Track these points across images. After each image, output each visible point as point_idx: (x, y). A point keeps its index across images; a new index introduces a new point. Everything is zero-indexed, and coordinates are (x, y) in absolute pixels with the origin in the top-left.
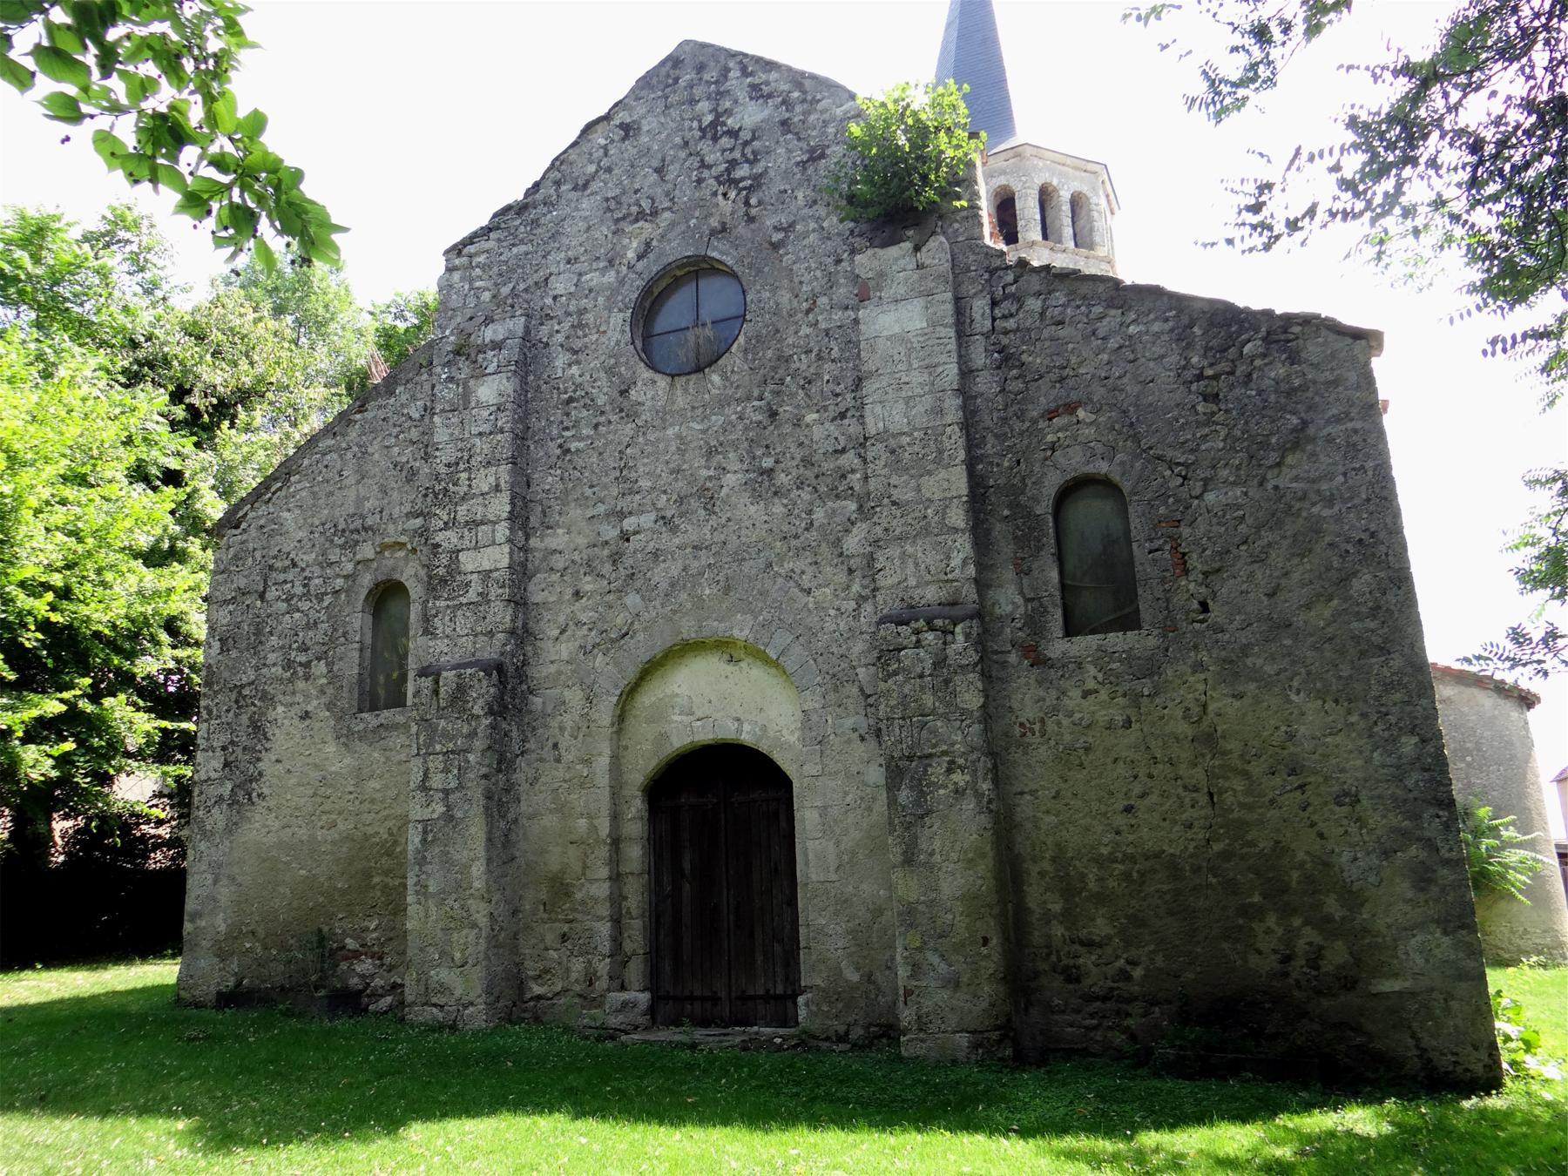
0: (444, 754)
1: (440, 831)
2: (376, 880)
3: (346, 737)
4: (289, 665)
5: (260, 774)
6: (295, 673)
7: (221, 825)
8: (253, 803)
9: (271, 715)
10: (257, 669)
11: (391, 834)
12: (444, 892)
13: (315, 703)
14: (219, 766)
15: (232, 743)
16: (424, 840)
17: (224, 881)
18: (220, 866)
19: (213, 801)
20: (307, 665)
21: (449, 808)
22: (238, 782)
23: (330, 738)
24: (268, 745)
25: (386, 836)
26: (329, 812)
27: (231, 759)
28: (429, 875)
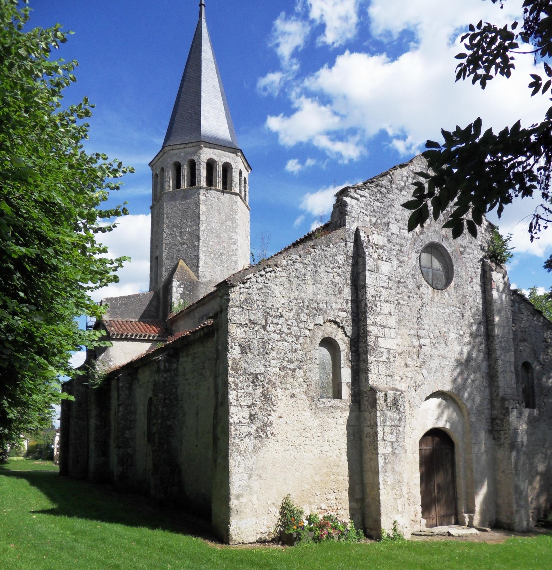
4: (282, 368)
5: (271, 423)
6: (287, 373)
7: (250, 448)
8: (269, 438)
14: (247, 415)
15: (253, 404)
16: (385, 462)
17: (254, 478)
19: (244, 435)
20: (294, 370)
24: (274, 408)
27: (253, 413)
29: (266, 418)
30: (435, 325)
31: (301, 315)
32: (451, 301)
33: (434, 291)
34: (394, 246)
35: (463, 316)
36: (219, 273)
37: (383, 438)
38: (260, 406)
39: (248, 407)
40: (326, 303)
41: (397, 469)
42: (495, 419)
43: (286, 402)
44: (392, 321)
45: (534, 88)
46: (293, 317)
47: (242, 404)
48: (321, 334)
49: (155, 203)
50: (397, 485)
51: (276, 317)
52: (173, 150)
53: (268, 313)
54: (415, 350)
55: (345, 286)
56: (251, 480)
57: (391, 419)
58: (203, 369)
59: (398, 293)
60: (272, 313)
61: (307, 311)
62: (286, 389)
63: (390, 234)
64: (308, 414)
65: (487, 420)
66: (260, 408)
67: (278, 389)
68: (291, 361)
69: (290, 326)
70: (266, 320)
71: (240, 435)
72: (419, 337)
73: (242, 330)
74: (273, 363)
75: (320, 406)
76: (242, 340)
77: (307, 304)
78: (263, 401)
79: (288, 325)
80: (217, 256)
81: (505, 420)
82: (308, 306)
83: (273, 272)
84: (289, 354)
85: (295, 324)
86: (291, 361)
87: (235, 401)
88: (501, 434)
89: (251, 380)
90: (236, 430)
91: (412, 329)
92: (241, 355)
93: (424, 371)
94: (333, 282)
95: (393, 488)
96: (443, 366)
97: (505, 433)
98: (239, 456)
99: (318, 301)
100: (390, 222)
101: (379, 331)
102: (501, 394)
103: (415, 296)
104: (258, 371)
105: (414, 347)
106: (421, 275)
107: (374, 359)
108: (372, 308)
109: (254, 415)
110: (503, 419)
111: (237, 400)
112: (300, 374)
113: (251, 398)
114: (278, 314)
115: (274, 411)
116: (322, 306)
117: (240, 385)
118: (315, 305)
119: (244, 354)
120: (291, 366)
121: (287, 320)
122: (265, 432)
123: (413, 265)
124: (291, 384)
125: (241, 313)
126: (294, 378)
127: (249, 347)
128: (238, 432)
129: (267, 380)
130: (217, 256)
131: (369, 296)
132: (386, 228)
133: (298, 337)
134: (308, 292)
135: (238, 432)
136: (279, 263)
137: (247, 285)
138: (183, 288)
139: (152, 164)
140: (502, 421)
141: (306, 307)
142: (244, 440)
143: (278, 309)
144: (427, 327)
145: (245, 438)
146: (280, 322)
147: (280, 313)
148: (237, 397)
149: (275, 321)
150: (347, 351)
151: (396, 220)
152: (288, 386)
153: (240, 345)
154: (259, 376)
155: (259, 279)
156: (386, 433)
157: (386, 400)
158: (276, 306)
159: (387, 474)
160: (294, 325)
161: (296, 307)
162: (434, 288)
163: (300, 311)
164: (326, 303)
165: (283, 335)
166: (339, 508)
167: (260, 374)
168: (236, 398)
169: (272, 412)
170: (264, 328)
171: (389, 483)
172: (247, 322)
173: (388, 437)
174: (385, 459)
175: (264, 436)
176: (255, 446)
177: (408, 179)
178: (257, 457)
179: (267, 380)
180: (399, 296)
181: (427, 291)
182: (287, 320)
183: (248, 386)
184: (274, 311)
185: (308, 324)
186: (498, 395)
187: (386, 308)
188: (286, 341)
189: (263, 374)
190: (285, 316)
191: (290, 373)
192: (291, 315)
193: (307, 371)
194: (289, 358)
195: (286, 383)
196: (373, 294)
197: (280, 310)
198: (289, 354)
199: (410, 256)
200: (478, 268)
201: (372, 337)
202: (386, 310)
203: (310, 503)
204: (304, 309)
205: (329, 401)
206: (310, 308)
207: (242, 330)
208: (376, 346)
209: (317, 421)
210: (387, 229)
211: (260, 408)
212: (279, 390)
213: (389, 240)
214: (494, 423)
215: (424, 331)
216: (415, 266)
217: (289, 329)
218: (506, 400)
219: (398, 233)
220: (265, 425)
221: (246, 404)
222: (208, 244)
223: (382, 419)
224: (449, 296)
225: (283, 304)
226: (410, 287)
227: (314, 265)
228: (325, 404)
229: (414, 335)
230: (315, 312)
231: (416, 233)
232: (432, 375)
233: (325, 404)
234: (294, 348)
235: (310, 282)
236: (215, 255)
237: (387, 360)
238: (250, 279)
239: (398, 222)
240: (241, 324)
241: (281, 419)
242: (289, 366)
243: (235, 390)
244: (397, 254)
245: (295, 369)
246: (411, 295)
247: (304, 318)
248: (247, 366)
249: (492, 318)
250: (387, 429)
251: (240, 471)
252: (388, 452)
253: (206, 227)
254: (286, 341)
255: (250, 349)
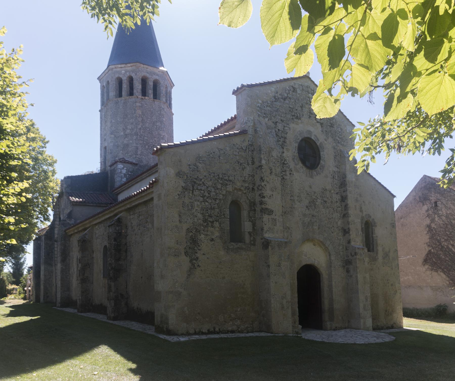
20: (212, 222)
24: (199, 248)
31: (217, 184)
34: (280, 139)
36: (152, 159)
45: (435, 5)
48: (231, 197)
49: (103, 107)
52: (116, 68)
53: (195, 182)
58: (147, 223)
59: (283, 171)
61: (221, 182)
62: (207, 235)
63: (277, 130)
68: (210, 216)
70: (193, 187)
75: (230, 247)
77: (221, 176)
80: (150, 147)
82: (222, 178)
85: (213, 190)
86: (210, 216)
100: (277, 122)
112: (217, 224)
115: (199, 250)
118: (227, 178)
121: (207, 187)
130: (150, 147)
131: (133, 323)
133: (215, 199)
138: (126, 169)
139: (100, 78)
143: (201, 179)
146: (203, 188)
149: (199, 187)
160: (213, 191)
163: (216, 181)
165: (205, 198)
177: (289, 92)
180: (284, 173)
182: (207, 187)
188: (207, 202)
194: (209, 213)
195: (207, 231)
204: (219, 180)
205: (237, 244)
206: (223, 180)
213: (277, 134)
217: (209, 194)
219: (283, 130)
222: (143, 138)
234: (212, 207)
236: (149, 146)
239: (283, 122)
242: (209, 219)
244: (282, 144)
253: (142, 126)
254: (207, 202)
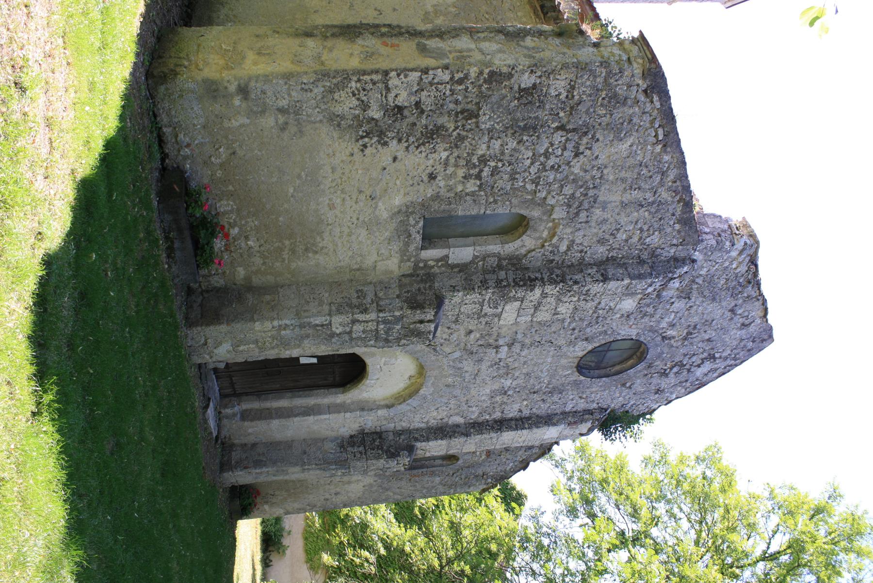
0: (377, 330)
1: (323, 332)
2: (287, 243)
3: (406, 211)
4: (483, 160)
5: (385, 144)
6: (475, 166)
7: (338, 109)
8: (357, 141)
9: (441, 147)
10: (490, 131)
11: (322, 248)
12: (281, 338)
13: (442, 184)
14: (400, 101)
15: (422, 112)
16: (317, 325)
17: (281, 119)
18: (296, 113)
19: (364, 98)
20: (478, 177)
21: (339, 335)
22: (381, 124)
23: (409, 198)
24: (412, 148)
25: (321, 245)
26: (343, 205)
27: (406, 112)
28: (293, 330)
29: (394, 135)
30: (525, 363)
32: (557, 378)
33: (577, 357)
35: (534, 393)
37: (358, 321)
38: (418, 123)
39: (418, 104)
40: (587, 222)
41: (306, 342)
42: (380, 437)
43: (423, 167)
44: (543, 316)
46: (573, 173)
47: (425, 93)
50: (279, 343)
51: (577, 147)
53: (586, 133)
54: (491, 341)
55: (609, 247)
56: (276, 112)
57: (389, 329)
60: (585, 140)
61: (578, 194)
64: (398, 201)
65: (378, 428)
66: (414, 124)
67: (446, 154)
69: (557, 170)
70: (574, 130)
71: (364, 90)
72: (510, 345)
73: (562, 90)
74: (497, 144)
75: (411, 219)
76: (545, 89)
78: (426, 128)
79: (559, 166)
81: (380, 452)
82: (586, 194)
83: (654, 140)
84: (509, 169)
87: (430, 79)
88: (359, 447)
89: (469, 106)
90: (374, 83)
91: (525, 335)
92: (516, 87)
93: (457, 354)
94: (618, 230)
95: (273, 338)
96: (463, 375)
97: (361, 453)
98: (323, 89)
99: (593, 210)
101: (532, 301)
102: (418, 445)
103: (573, 336)
104: (483, 119)
105: (496, 340)
106: (603, 342)
107: (487, 298)
108: (570, 291)
109: (402, 114)
110: (382, 449)
111: (431, 84)
113: (433, 108)
114: (582, 148)
115: (407, 148)
116: (583, 215)
117: (460, 88)
118: (586, 205)
119: (517, 95)
120: (486, 172)
122: (368, 134)
123: (620, 332)
124: (454, 174)
125: (593, 87)
126: (465, 177)
127: (530, 102)
128: (369, 86)
129: (465, 133)
132: (683, 295)
133: (536, 182)
134: (612, 195)
135: (369, 86)
136: (669, 149)
137: (642, 98)
140: (378, 449)
141: (584, 192)
142: (354, 99)
143: (590, 149)
144: (523, 354)
145: (358, 99)
147: (582, 153)
148: (438, 83)
150: (502, 253)
151: (691, 307)
152: (450, 170)
153: (534, 86)
154: (474, 120)
155: (647, 118)
156: (366, 324)
157: (421, 322)
158: (596, 146)
159: (297, 329)
160: (558, 175)
161: (588, 177)
162: (581, 358)
163: (580, 183)
164: (587, 222)
165: (542, 159)
166: (233, 254)
167: (477, 123)
168: (435, 81)
169: (406, 144)
170: (562, 128)
171: (283, 332)
172: (577, 98)
173: (358, 328)
174: (322, 326)
175: (361, 133)
176: (343, 117)
178: (321, 121)
179: (465, 133)
181: (577, 349)
183: (457, 102)
184: (587, 143)
185: (557, 197)
186: (417, 440)
187: (565, 309)
188: (532, 164)
189: (478, 127)
190: (576, 160)
191: (474, 172)
192: (576, 170)
193: (475, 198)
196: (591, 291)
197: (588, 152)
198: (509, 169)
199: (634, 326)
200: (598, 404)
201: (523, 294)
202: (562, 309)
203: (238, 210)
204: (582, 190)
206: (582, 198)
207: (562, 90)
208: (509, 300)
209: (385, 215)
210: (681, 297)
211: (414, 124)
212: (444, 155)
214: (375, 436)
215: (518, 351)
216: (619, 334)
217: (552, 167)
218: (409, 452)
220: (381, 134)
221: (423, 98)
223: (390, 318)
224: (565, 376)
225: (597, 157)
226: (588, 330)
227: (653, 203)
228: (414, 226)
229: (515, 339)
230: (575, 206)
231: (665, 332)
232: (451, 363)
233: (414, 226)
234: (517, 176)
235: (627, 197)
237: (483, 313)
238: (652, 102)
240: (573, 88)
241: (390, 159)
242: (486, 169)
243: (452, 79)
245: (480, 179)
246: (576, 331)
247: (568, 190)
248: (494, 99)
249: (527, 426)
250: (371, 326)
251: (294, 94)
252: (334, 329)
254: (532, 164)
255: (525, 105)
